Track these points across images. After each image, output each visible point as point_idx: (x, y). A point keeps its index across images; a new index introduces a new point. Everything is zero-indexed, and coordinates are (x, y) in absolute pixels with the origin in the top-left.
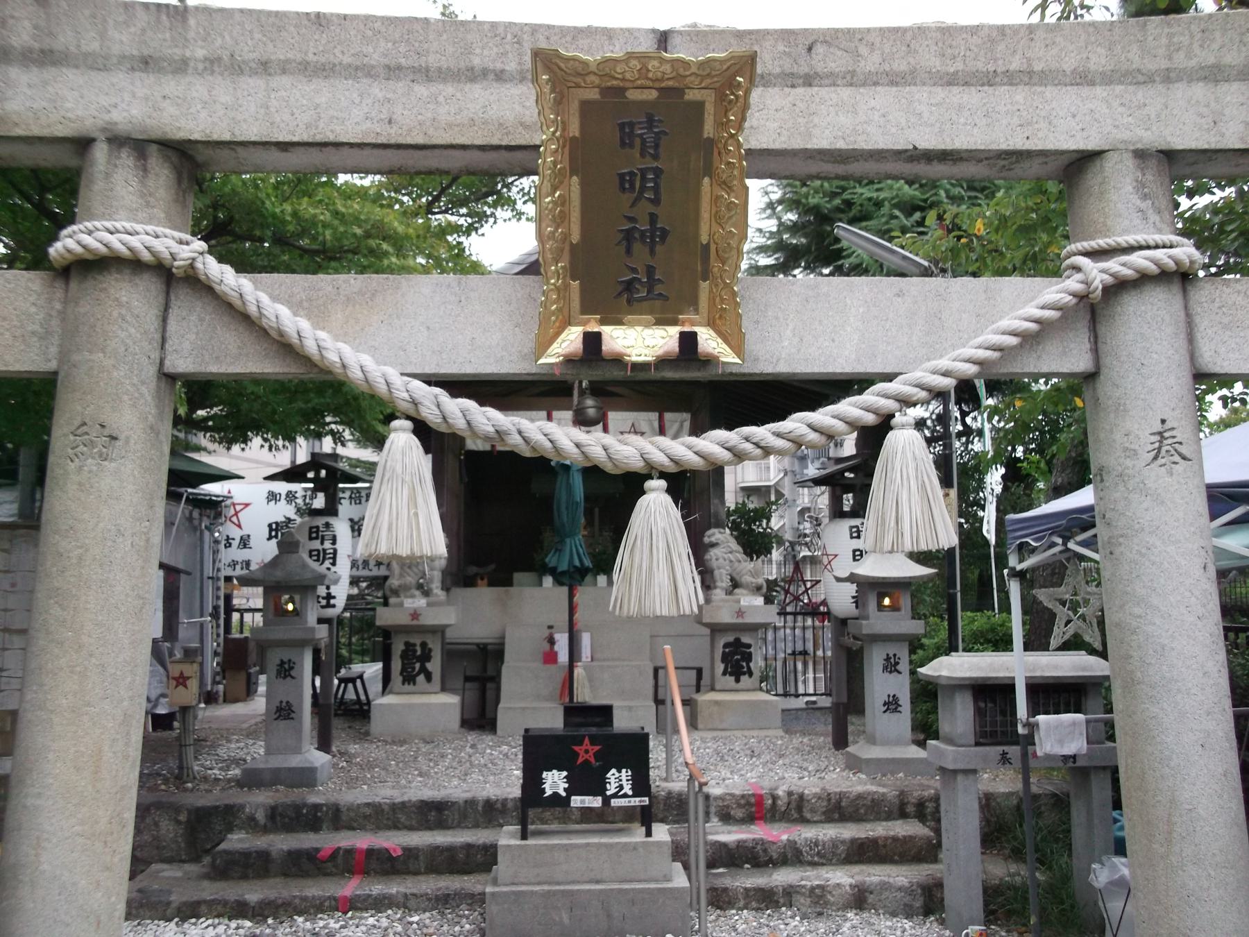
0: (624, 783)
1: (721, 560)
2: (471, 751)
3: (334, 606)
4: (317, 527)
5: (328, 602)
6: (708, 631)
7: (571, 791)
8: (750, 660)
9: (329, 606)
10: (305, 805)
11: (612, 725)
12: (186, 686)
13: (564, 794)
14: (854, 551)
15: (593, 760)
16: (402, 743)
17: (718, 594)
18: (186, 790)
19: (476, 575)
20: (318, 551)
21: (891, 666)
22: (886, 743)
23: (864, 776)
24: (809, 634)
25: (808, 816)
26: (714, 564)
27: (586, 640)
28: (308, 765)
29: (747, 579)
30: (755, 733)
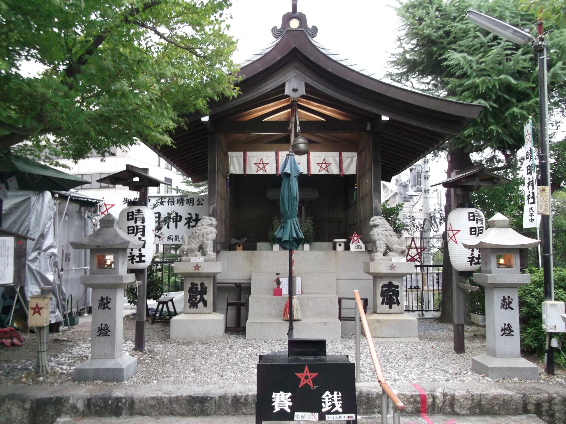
0: (336, 402)
1: (380, 235)
2: (229, 351)
3: (144, 261)
4: (133, 212)
5: (140, 259)
6: (372, 277)
7: (294, 409)
8: (398, 296)
9: (140, 261)
10: (110, 398)
11: (324, 353)
12: (40, 314)
13: (289, 411)
14: (471, 228)
15: (311, 384)
16: (189, 343)
17: (379, 255)
18: (38, 383)
19: (236, 243)
20: (133, 227)
21: (506, 304)
22: (503, 356)
23: (490, 379)
24: (420, 277)
25: (458, 410)
26: (376, 237)
27: (298, 282)
28: (117, 367)
29: (396, 246)
30: (402, 340)
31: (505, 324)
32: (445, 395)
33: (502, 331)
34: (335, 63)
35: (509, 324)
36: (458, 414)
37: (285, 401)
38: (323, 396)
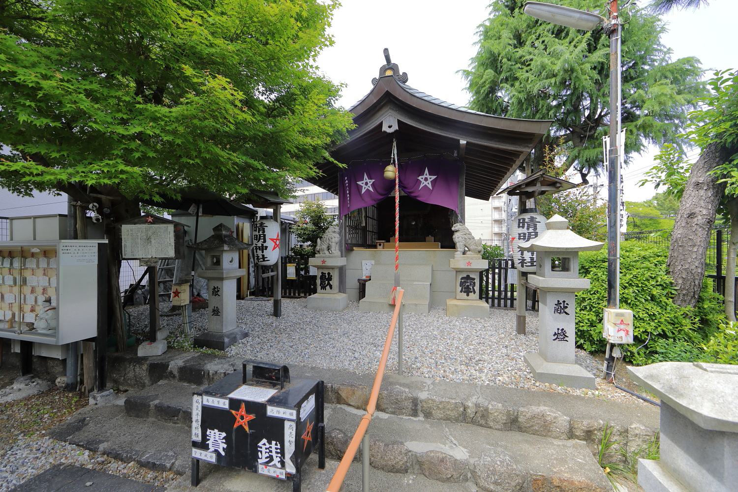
9: (264, 261)
25: (491, 424)
31: (558, 329)
32: (477, 405)
33: (554, 335)
34: (419, 99)
35: (563, 329)
36: (491, 428)
37: (220, 441)
38: (260, 444)
